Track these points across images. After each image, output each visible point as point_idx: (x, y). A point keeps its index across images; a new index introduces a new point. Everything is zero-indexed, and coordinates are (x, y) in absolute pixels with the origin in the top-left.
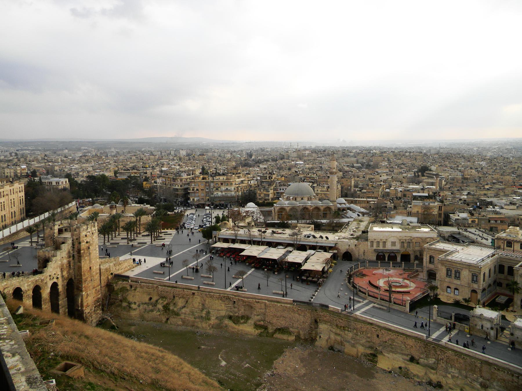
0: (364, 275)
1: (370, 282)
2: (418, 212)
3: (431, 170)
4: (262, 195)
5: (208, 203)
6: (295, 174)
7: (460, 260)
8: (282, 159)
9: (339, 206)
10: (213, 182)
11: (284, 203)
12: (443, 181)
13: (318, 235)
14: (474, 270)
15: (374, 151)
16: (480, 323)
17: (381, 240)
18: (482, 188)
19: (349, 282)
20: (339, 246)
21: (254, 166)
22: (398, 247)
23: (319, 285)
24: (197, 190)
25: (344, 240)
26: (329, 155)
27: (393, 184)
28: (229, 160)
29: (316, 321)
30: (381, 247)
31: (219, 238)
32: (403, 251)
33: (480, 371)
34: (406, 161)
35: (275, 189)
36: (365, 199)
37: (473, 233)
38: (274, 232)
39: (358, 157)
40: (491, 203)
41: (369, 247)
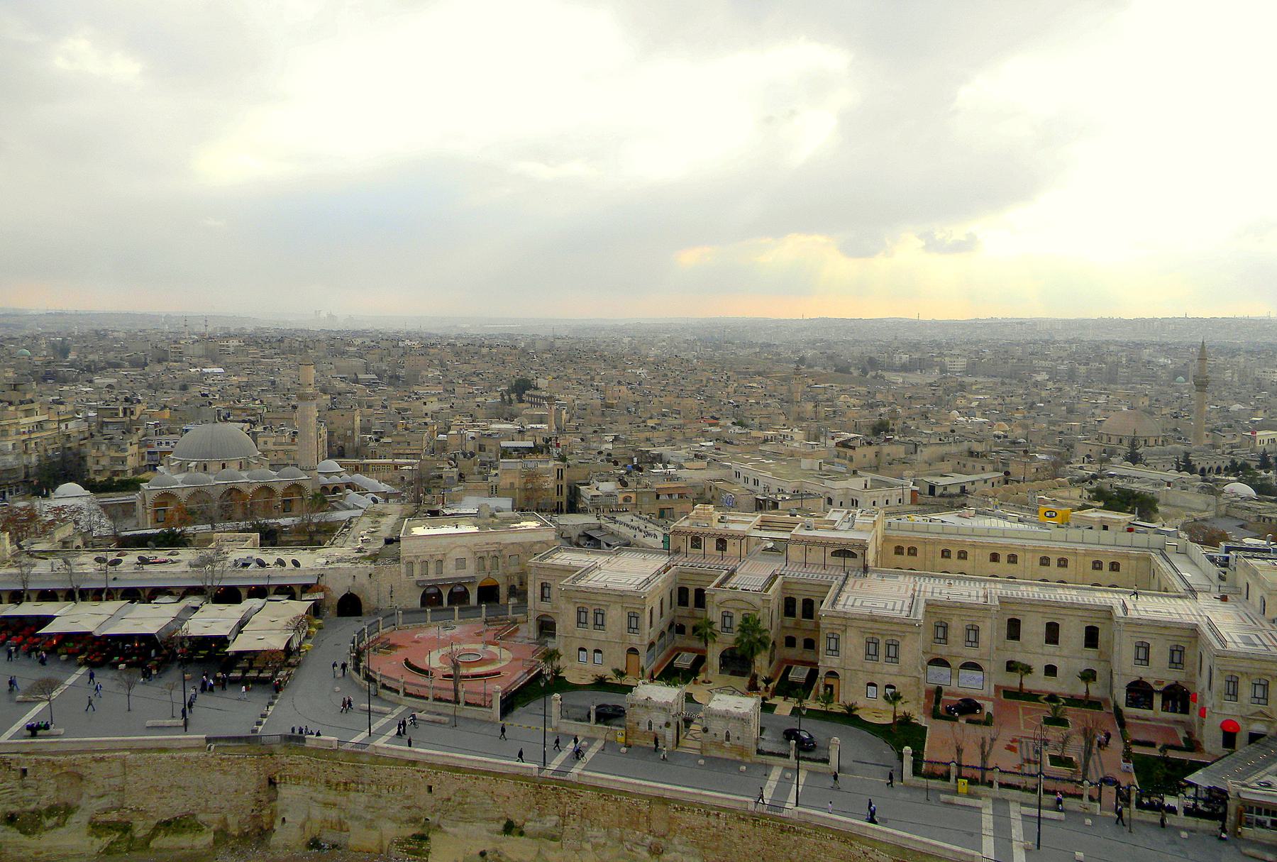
0: (393, 647)
1: (407, 663)
2: (512, 484)
3: (536, 388)
8: (159, 361)
9: (324, 480)
11: (171, 478)
13: (270, 557)
15: (407, 342)
20: (328, 582)
21: (75, 381)
22: (470, 570)
25: (341, 565)
26: (292, 351)
29: (272, 782)
32: (481, 579)
35: (143, 444)
38: (143, 561)
40: (659, 458)
41: (404, 576)
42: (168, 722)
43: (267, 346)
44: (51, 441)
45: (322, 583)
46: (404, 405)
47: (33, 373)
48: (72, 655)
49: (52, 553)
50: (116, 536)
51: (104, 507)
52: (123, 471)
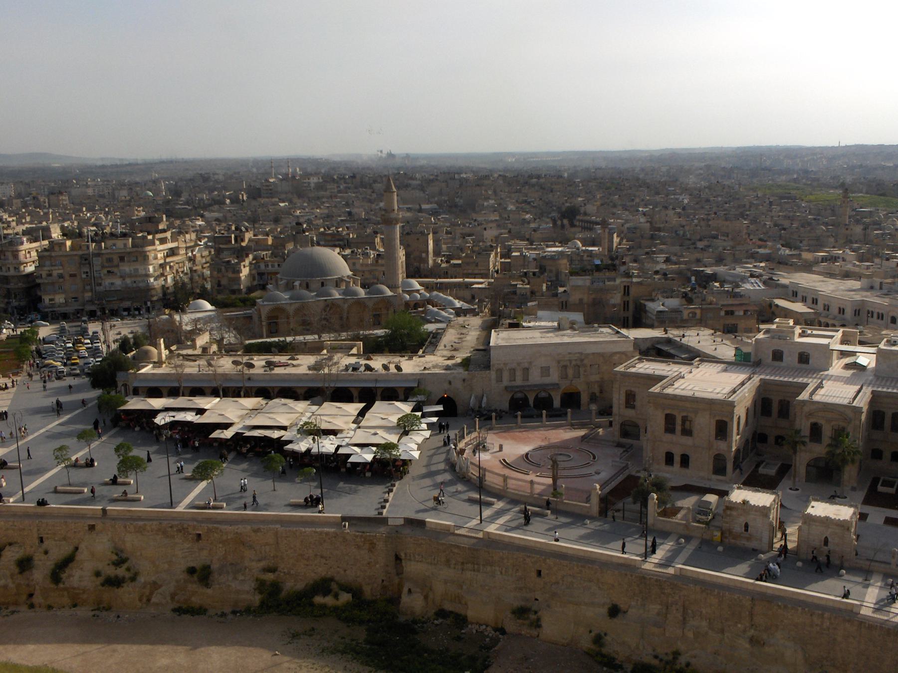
2: (581, 300)
3: (585, 214)
7: (690, 394)
12: (615, 235)
14: (719, 412)
16: (742, 520)
17: (519, 364)
18: (692, 246)
22: (554, 377)
29: (398, 558)
30: (519, 382)
32: (564, 385)
33: (751, 615)
37: (699, 338)
40: (714, 277)
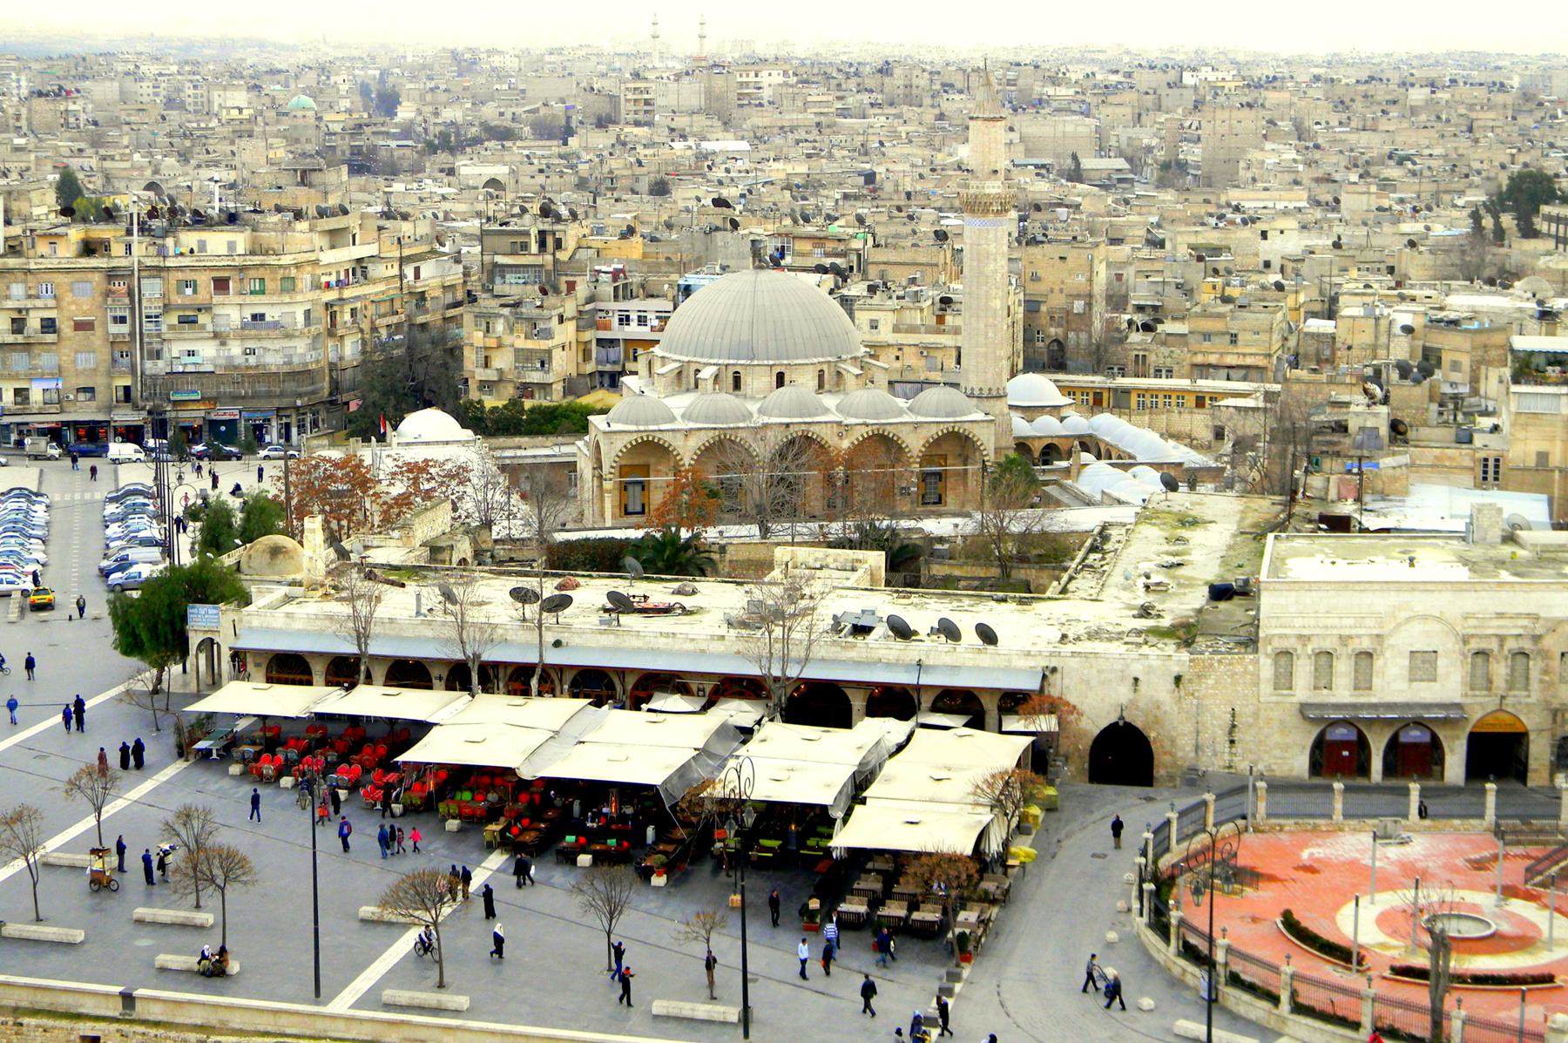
0: (1249, 876)
1: (1292, 925)
2: (1543, 457)
4: (503, 361)
5: (126, 416)
6: (717, 217)
8: (602, 123)
9: (1021, 426)
10: (158, 271)
11: (650, 405)
13: (923, 612)
15: (1206, 73)
19: (1161, 926)
20: (1067, 687)
21: (416, 170)
22: (1448, 686)
23: (963, 949)
24: (49, 325)
25: (1097, 646)
26: (912, 99)
27: (1350, 282)
28: (243, 132)
30: (1342, 693)
31: (238, 656)
34: (1409, 139)
35: (588, 319)
36: (1184, 383)
38: (620, 604)
39: (1105, 110)
41: (1266, 688)
42: (703, 1010)
43: (852, 84)
44: (384, 308)
45: (1054, 691)
46: (1210, 237)
47: (327, 152)
48: (472, 822)
49: (414, 571)
50: (542, 539)
51: (512, 471)
52: (545, 387)
